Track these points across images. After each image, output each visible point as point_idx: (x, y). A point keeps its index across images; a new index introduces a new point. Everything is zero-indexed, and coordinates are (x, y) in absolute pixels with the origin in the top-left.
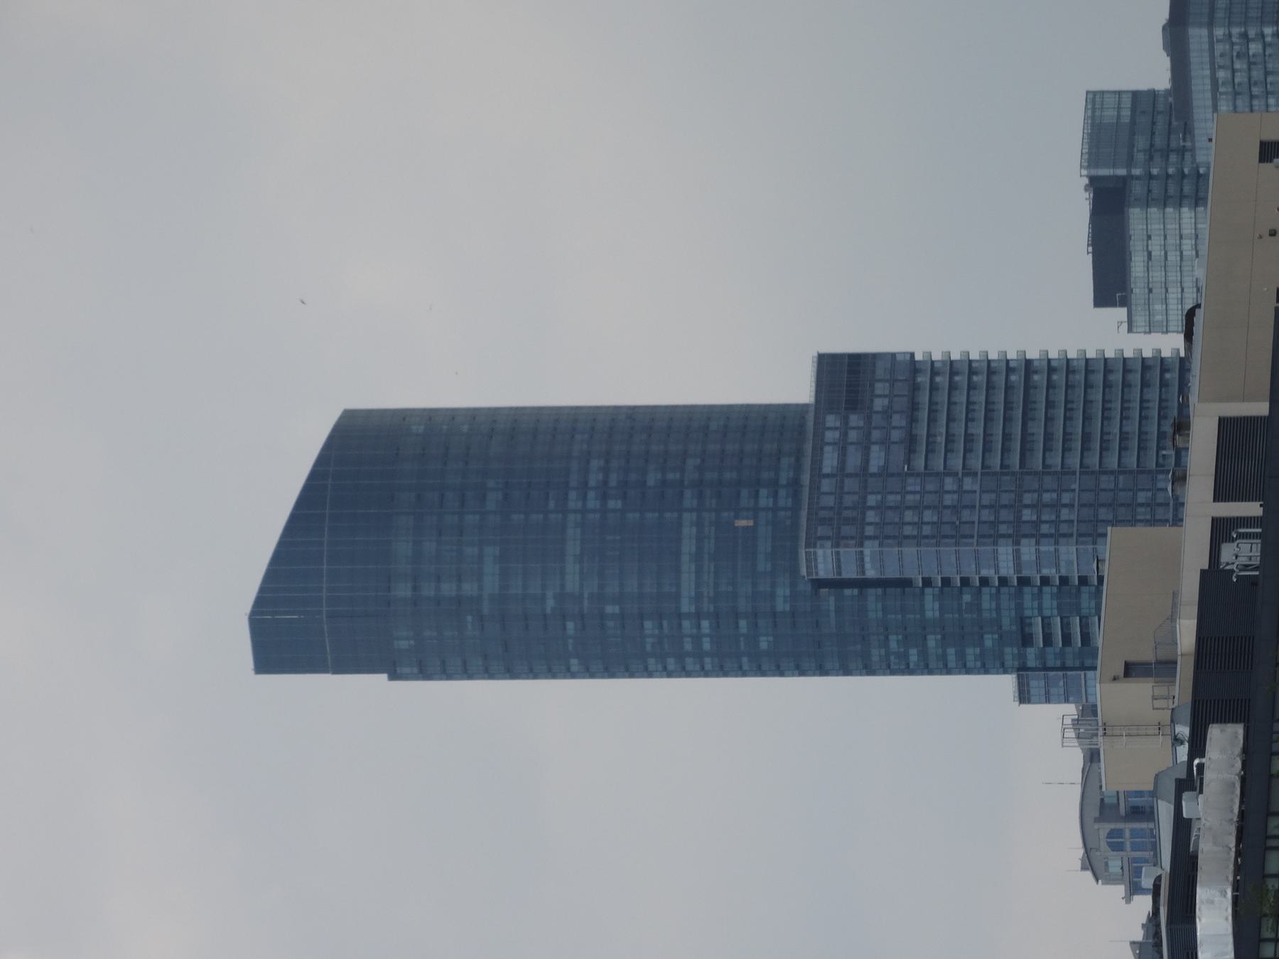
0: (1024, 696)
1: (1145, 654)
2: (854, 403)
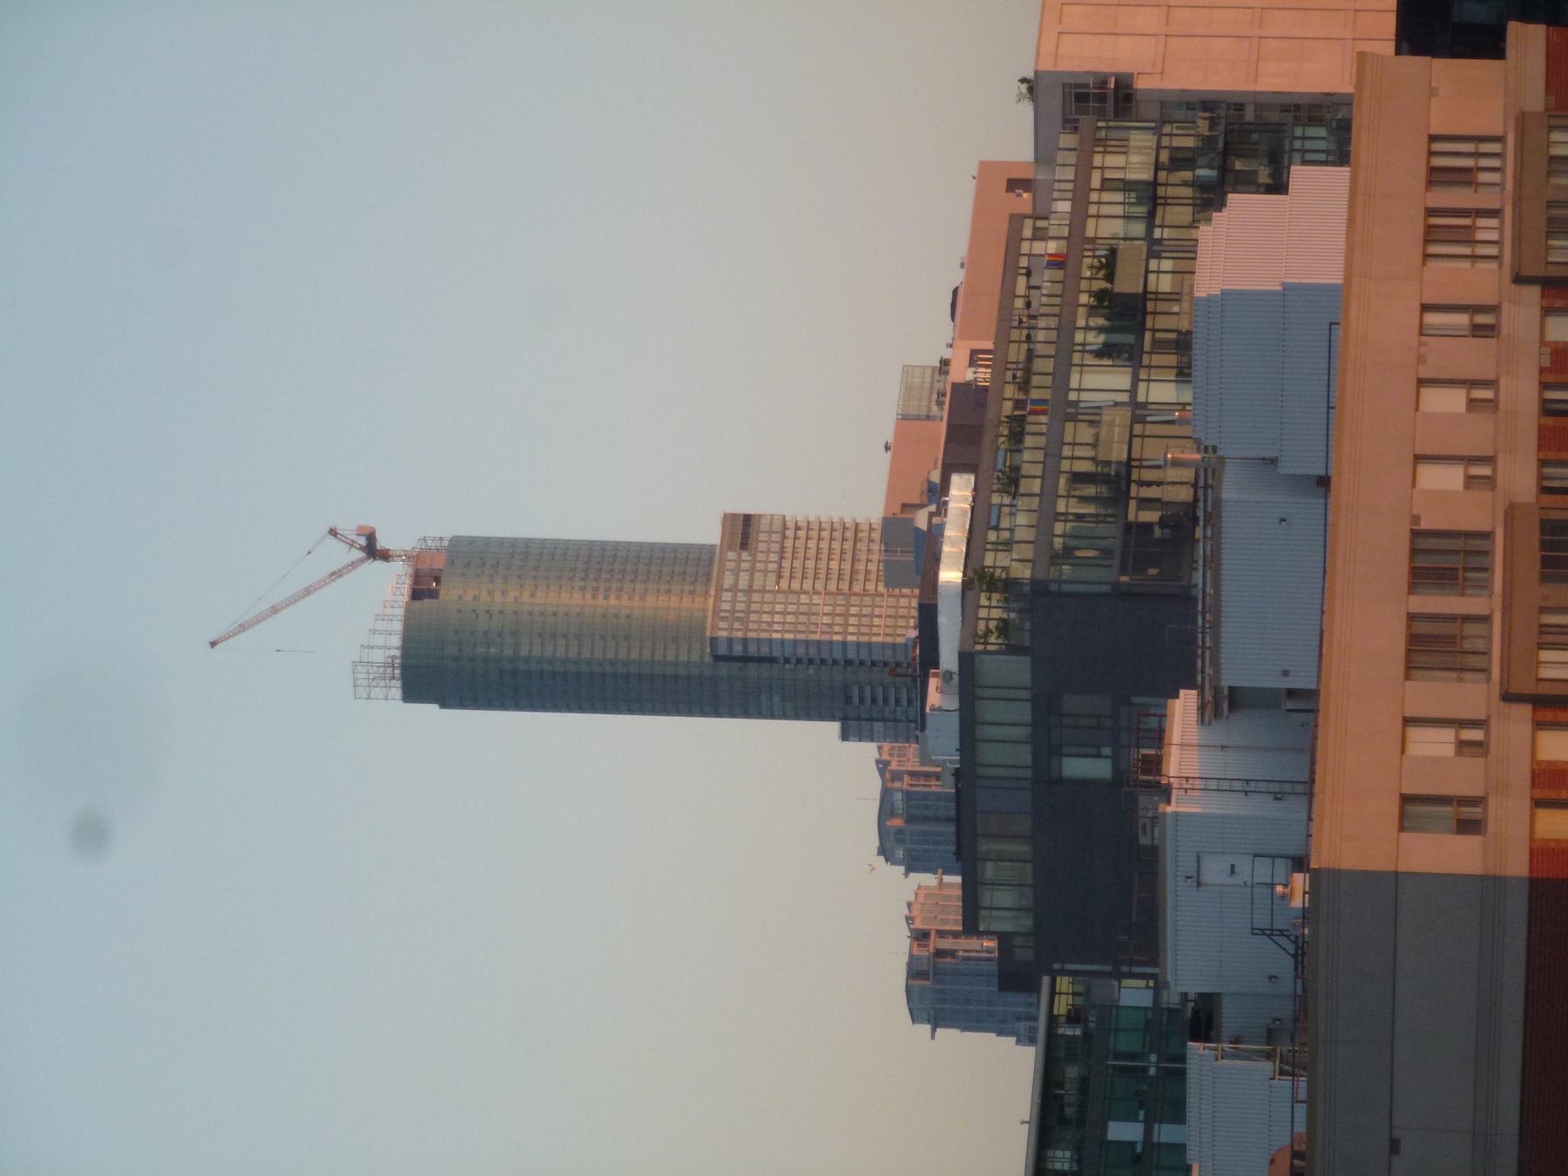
0: (845, 736)
2: (744, 545)
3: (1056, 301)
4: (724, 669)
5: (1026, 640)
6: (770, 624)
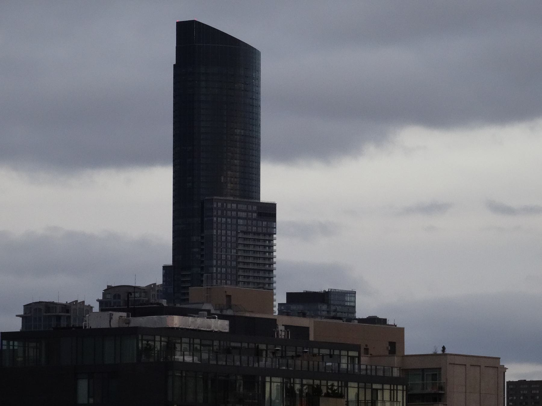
0: (165, 268)
1: (233, 302)
2: (260, 214)
3: (316, 370)
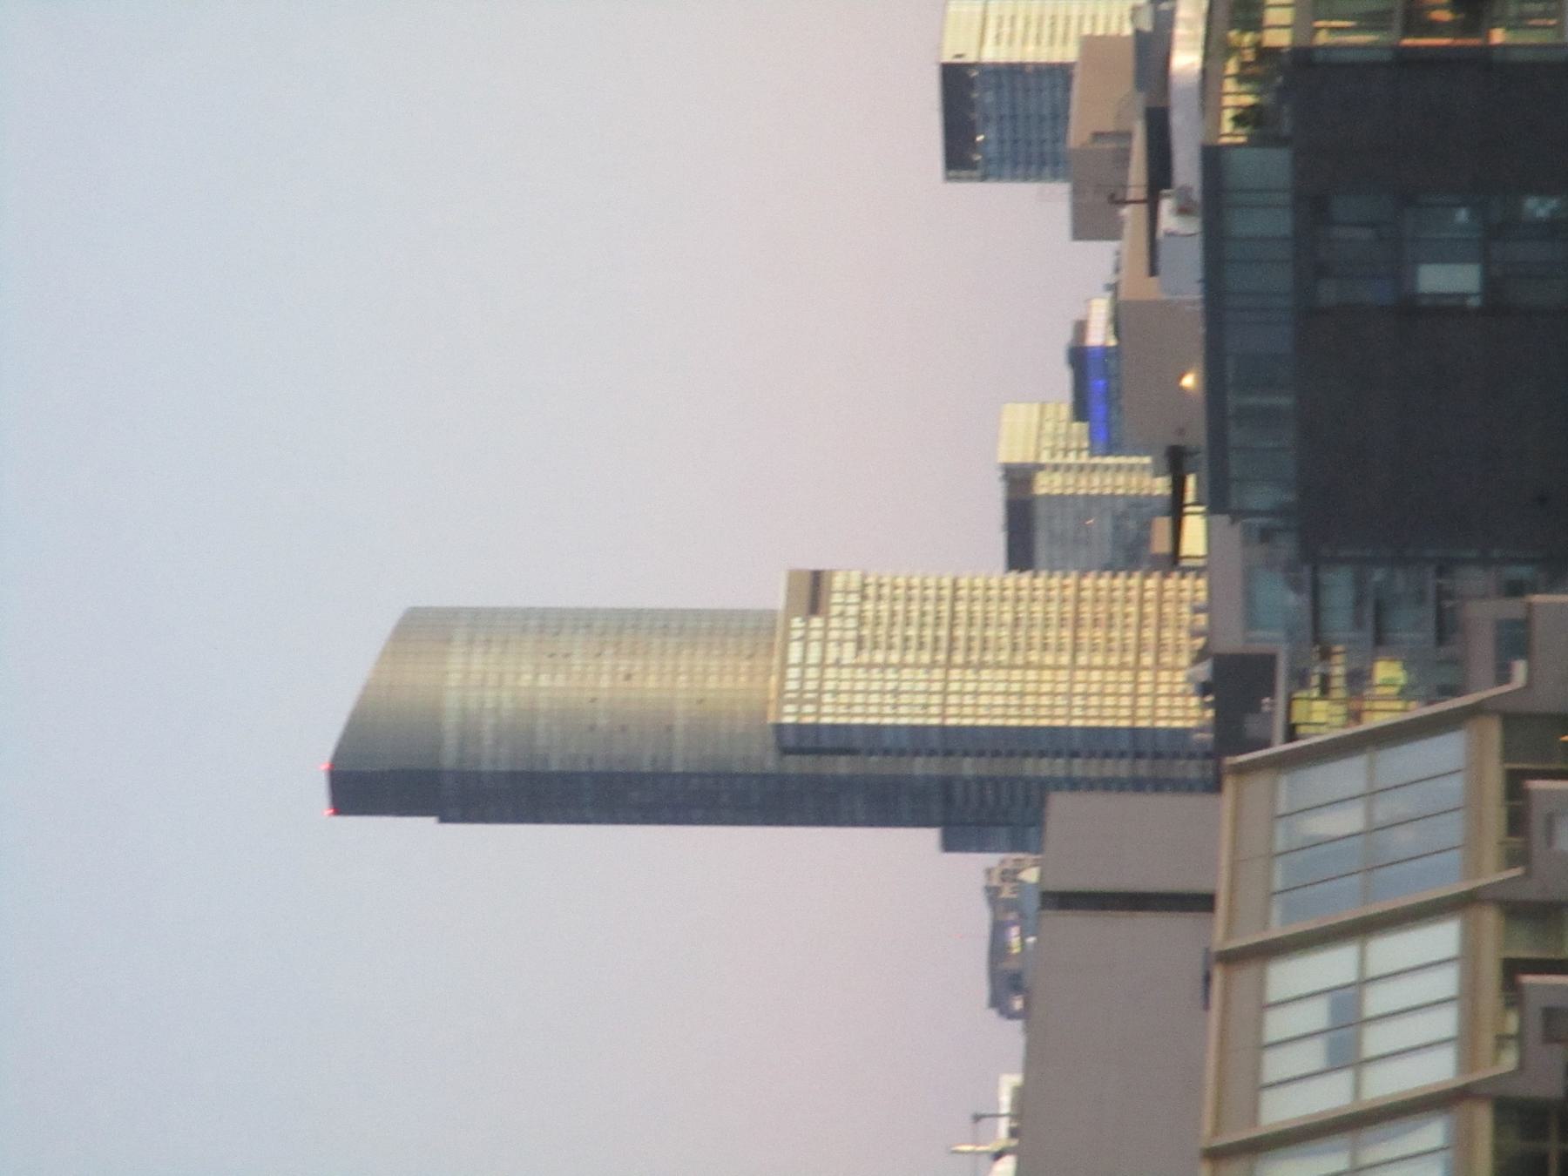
0: (949, 845)
4: (793, 765)
5: (1286, 127)
6: (850, 705)
